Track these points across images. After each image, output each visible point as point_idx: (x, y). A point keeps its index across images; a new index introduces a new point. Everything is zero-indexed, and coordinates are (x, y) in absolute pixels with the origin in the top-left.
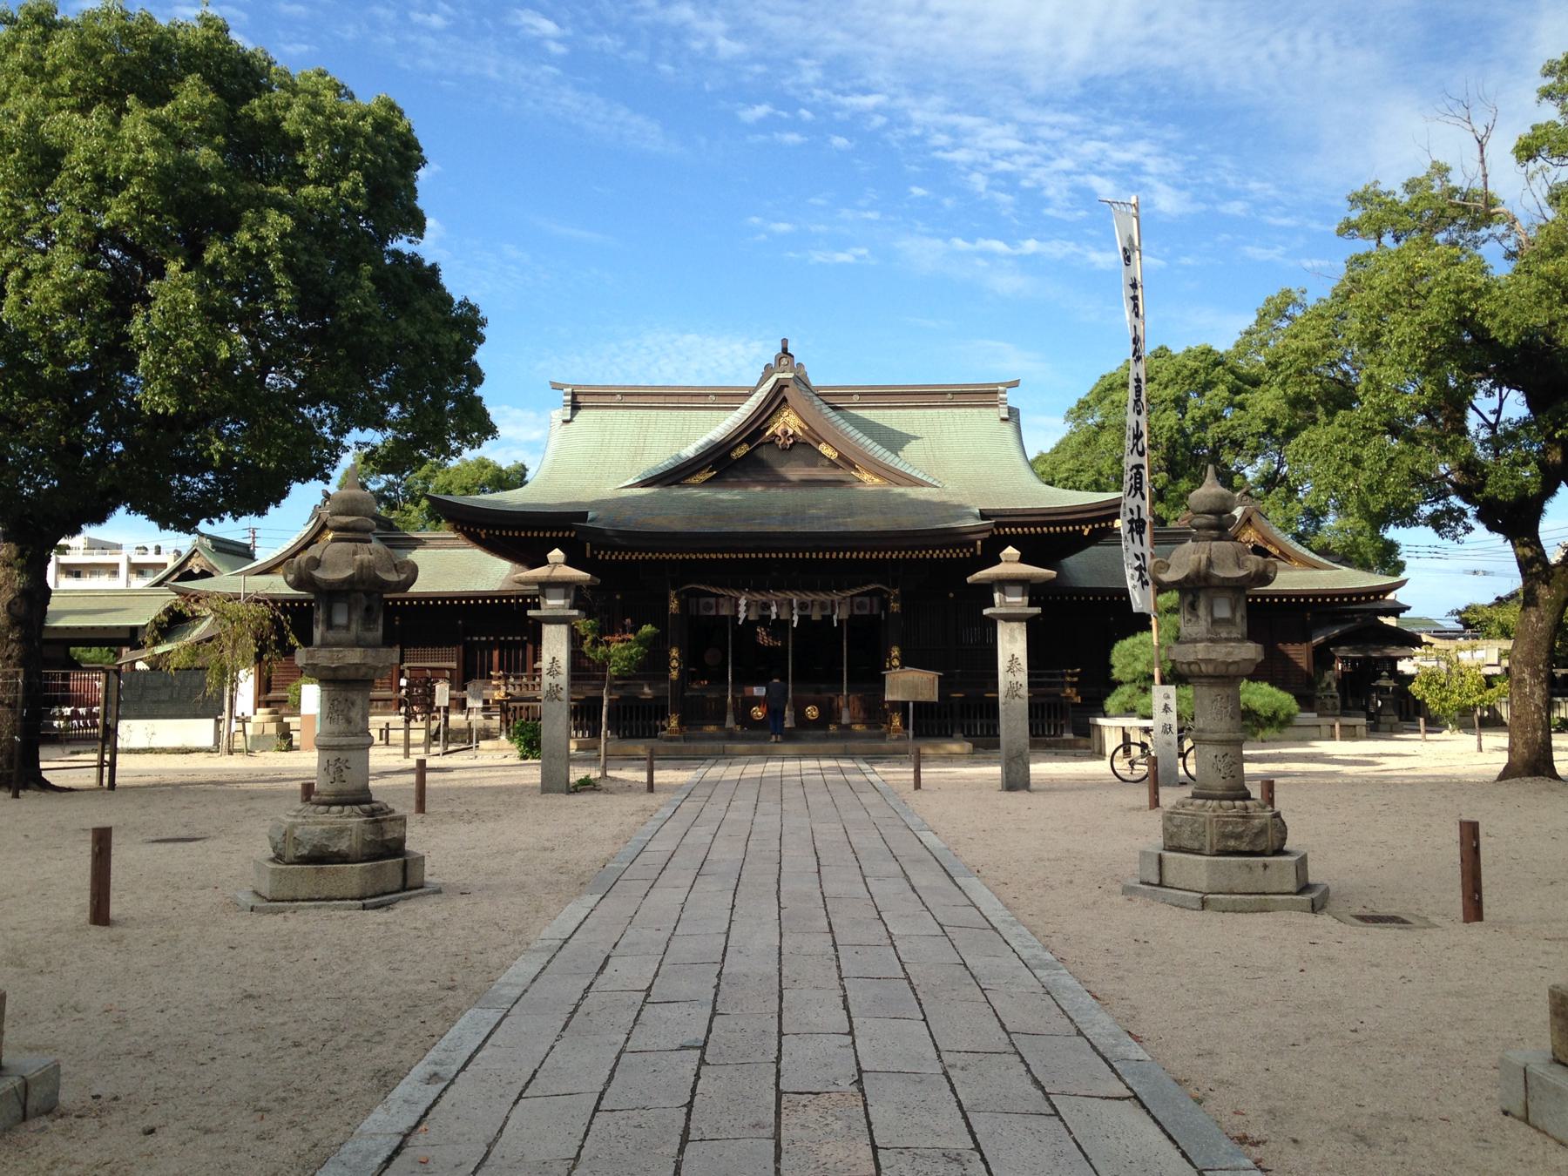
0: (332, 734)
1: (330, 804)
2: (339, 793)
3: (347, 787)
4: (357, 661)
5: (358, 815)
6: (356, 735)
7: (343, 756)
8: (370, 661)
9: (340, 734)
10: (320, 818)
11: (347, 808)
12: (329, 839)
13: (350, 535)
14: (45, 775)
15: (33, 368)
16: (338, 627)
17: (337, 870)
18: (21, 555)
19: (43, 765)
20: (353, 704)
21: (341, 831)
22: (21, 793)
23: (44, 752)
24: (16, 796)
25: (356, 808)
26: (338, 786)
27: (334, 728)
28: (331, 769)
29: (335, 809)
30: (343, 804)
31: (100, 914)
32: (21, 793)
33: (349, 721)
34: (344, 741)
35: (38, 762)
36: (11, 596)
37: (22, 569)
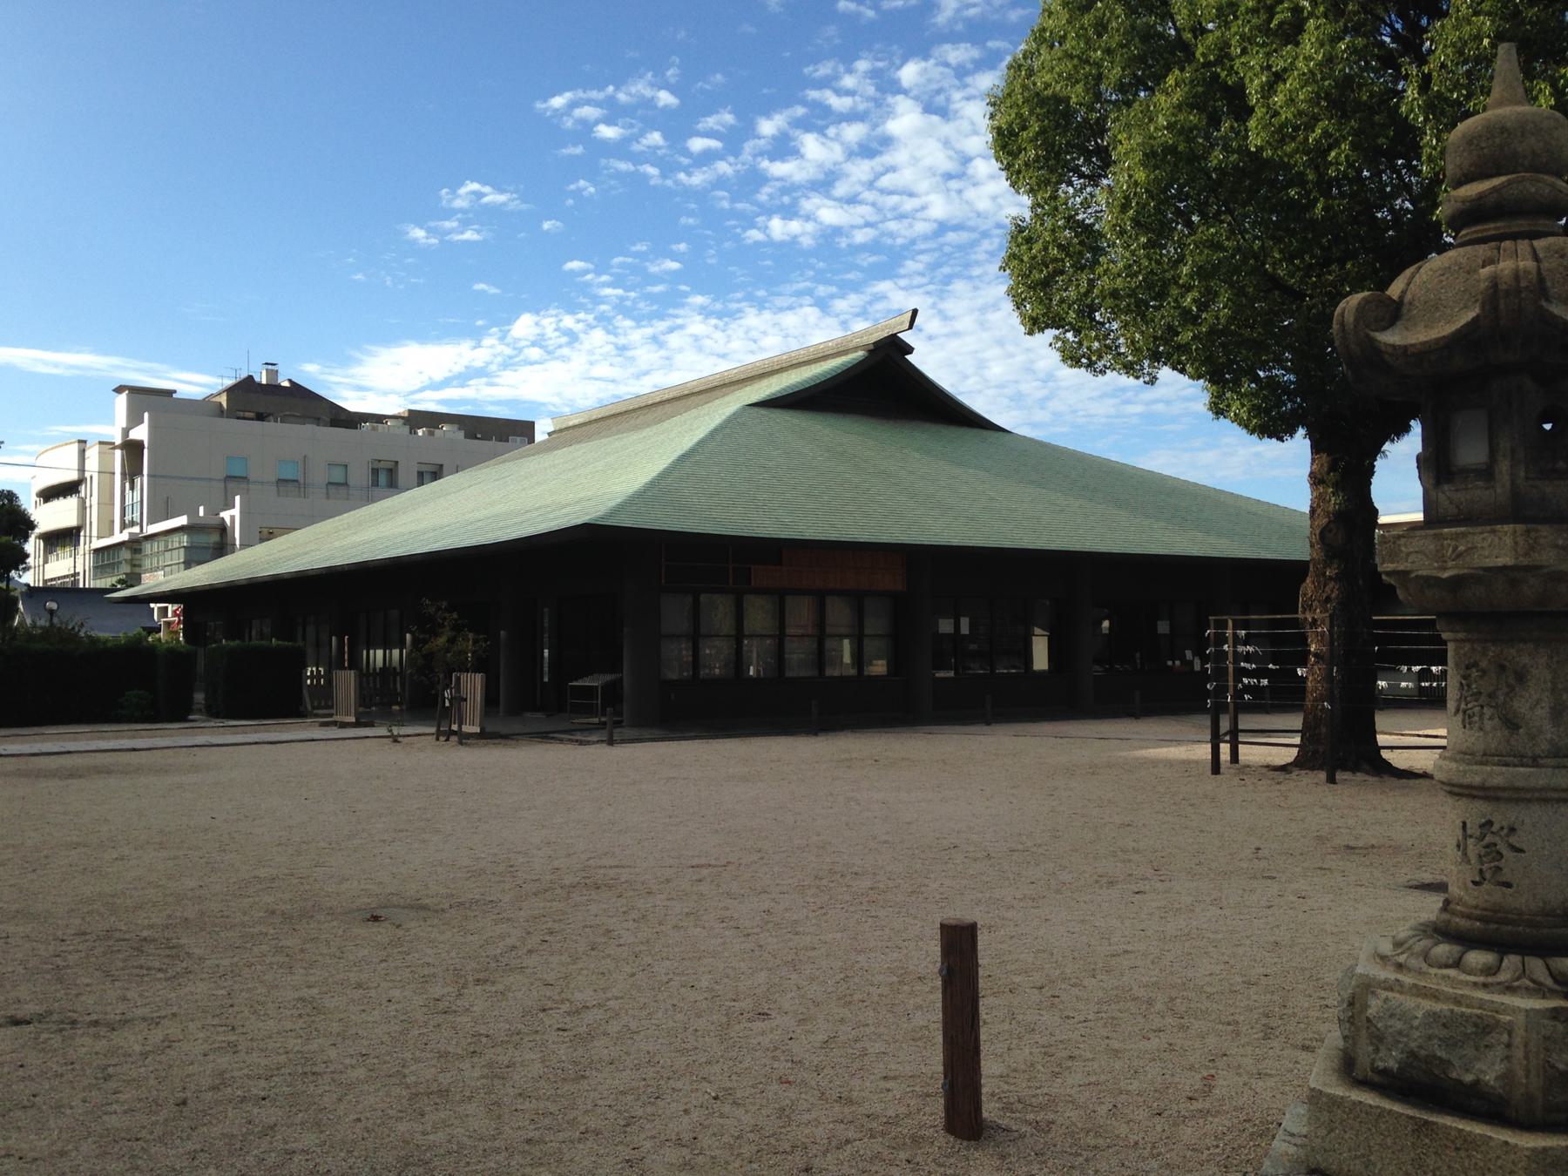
0: (1485, 758)
1: (1468, 941)
2: (1494, 915)
3: (1521, 900)
4: (1505, 560)
5: (1539, 990)
6: (1535, 761)
7: (1503, 816)
8: (1547, 557)
9: (1485, 758)
10: (1434, 978)
11: (1512, 961)
12: (1450, 1043)
13: (1491, 228)
14: (1385, 754)
15: (1299, 209)
16: (1466, 472)
17: (1468, 1143)
18: (1333, 467)
19: (1382, 739)
20: (1521, 677)
21: (1484, 1028)
22: (1339, 776)
23: (1382, 720)
24: (1331, 780)
25: (1536, 966)
26: (1491, 895)
27: (1473, 739)
28: (1473, 848)
29: (1477, 958)
30: (1500, 945)
31: (964, 1115)
32: (1339, 776)
33: (1511, 723)
34: (1498, 776)
35: (1374, 733)
36: (1325, 521)
37: (1337, 486)
